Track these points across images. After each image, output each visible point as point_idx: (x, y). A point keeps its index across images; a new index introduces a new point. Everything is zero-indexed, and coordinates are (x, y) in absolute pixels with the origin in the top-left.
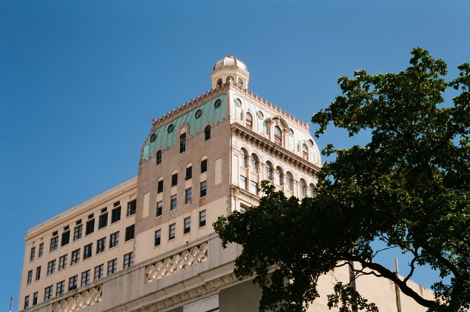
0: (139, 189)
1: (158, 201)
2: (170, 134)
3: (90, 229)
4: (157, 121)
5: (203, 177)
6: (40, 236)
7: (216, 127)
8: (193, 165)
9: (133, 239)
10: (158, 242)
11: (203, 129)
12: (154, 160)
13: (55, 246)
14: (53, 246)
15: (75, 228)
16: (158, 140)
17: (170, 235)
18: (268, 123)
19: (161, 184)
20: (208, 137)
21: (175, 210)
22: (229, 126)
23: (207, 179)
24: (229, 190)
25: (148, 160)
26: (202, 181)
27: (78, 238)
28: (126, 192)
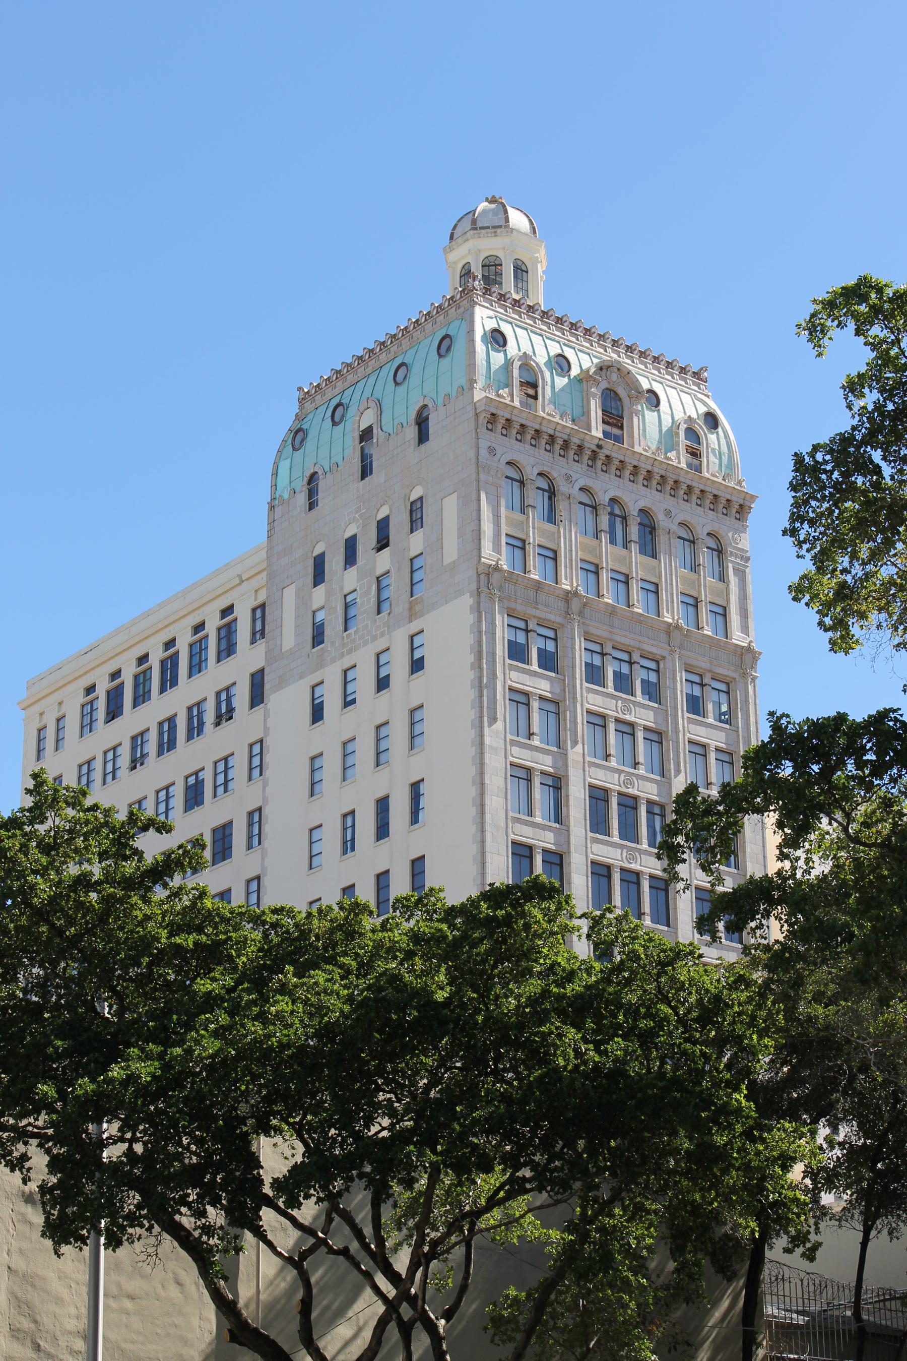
0: (271, 577)
1: (314, 608)
2: (297, 453)
3: (169, 680)
4: (308, 392)
5: (416, 542)
6: (57, 697)
7: (442, 410)
8: (391, 510)
9: (262, 705)
10: (317, 713)
11: (413, 415)
12: (302, 499)
13: (91, 722)
14: (87, 725)
15: (219, 629)
16: (310, 444)
17: (345, 696)
18: (585, 383)
19: (319, 563)
20: (423, 436)
21: (355, 632)
22: (470, 408)
23: (425, 548)
24: (475, 576)
25: (289, 499)
26: (413, 554)
27: (229, 656)
28: (247, 579)
